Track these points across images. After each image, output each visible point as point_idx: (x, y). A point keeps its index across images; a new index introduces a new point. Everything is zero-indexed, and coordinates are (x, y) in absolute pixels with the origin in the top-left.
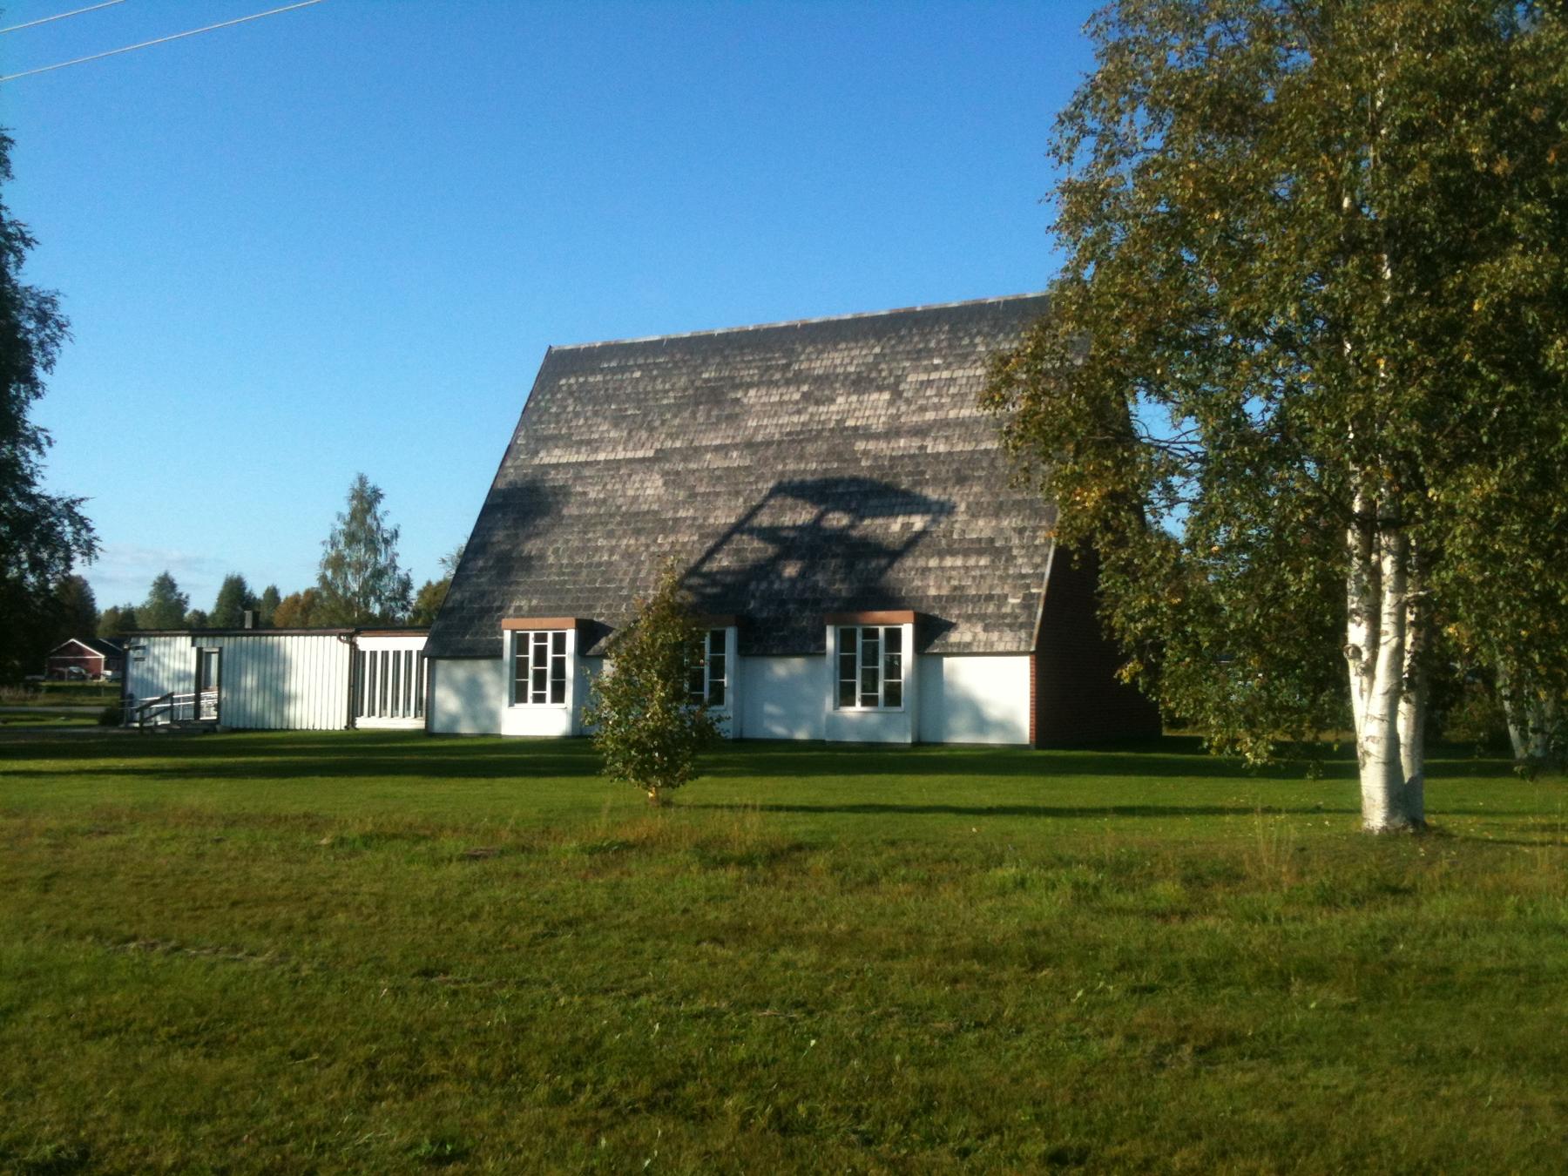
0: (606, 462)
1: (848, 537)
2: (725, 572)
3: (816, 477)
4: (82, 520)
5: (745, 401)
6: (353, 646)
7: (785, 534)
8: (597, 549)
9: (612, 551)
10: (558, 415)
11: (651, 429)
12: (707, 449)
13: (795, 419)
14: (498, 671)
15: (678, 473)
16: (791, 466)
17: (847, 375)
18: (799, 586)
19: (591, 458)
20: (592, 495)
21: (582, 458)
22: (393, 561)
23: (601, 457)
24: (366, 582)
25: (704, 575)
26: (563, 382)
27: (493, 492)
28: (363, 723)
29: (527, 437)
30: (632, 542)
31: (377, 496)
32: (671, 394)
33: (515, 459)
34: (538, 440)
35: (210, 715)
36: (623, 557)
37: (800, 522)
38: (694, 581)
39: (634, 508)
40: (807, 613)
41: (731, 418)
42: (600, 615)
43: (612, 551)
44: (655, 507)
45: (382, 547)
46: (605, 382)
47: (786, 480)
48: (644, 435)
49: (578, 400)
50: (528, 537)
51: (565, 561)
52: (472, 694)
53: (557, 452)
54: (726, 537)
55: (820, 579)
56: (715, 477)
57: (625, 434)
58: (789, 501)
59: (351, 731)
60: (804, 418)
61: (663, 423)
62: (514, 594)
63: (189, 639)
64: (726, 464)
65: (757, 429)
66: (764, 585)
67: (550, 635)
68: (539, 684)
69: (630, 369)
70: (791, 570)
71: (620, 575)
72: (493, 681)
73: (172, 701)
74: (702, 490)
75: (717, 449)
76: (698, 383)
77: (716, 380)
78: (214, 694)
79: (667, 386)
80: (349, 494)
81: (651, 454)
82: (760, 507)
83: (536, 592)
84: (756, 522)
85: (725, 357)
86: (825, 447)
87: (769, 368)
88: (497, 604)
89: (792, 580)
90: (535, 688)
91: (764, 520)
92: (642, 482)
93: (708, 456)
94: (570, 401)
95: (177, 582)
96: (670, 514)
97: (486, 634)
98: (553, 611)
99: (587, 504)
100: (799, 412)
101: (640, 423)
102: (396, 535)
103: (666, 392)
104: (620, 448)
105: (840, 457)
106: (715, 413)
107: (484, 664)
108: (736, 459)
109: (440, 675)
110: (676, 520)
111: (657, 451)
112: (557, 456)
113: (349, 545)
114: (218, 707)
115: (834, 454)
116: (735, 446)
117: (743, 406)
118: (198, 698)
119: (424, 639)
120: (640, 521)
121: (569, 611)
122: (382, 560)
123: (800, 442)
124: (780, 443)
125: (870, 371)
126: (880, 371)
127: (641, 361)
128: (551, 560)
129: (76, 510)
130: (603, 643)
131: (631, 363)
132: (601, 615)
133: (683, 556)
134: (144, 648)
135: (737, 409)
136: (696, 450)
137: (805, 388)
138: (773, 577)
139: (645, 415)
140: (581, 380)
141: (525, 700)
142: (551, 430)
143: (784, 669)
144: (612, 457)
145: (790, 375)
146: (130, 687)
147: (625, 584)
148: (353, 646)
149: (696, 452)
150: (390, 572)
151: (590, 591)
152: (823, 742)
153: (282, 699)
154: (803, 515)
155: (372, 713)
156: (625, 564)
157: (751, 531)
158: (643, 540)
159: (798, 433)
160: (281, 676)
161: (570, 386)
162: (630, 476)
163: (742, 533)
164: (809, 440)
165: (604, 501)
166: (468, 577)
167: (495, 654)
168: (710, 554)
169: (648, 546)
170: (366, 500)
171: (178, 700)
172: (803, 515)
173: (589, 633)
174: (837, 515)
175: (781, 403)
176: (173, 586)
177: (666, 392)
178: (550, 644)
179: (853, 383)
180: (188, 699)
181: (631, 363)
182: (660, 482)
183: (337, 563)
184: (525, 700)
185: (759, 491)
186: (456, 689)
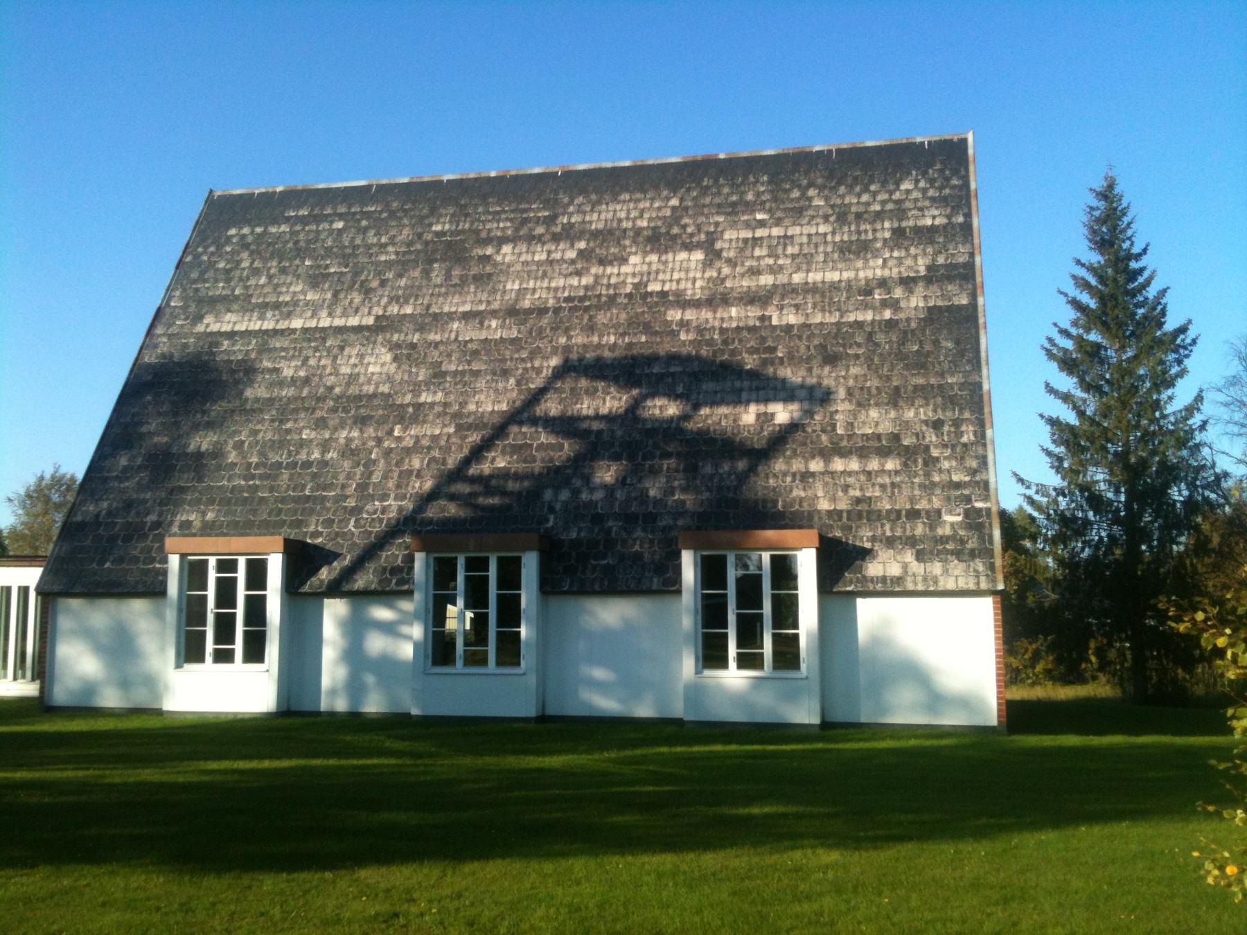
14: (160, 616)
50: (196, 427)
52: (119, 649)
62: (178, 504)
68: (225, 629)
72: (151, 628)
83: (211, 501)
88: (152, 518)
109: (64, 622)
128: (232, 457)
130: (325, 574)
165: (307, 381)
167: (155, 590)
178: (241, 575)
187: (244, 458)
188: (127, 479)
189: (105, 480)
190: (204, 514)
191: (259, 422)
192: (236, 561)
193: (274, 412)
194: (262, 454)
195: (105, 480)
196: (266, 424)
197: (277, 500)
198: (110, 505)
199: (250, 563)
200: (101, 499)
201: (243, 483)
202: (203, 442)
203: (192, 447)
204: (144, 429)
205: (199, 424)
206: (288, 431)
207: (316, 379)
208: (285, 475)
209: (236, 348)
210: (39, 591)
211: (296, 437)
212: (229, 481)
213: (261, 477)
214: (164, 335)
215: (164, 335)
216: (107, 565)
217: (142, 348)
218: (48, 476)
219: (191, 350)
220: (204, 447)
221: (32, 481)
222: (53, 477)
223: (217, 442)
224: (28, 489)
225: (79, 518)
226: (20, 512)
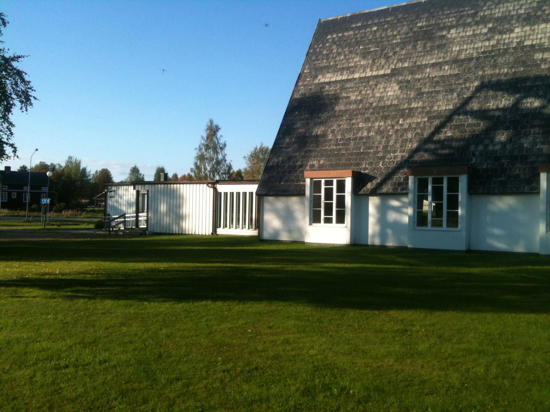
0: (360, 78)
1: (541, 114)
2: (451, 139)
3: (508, 77)
4: (19, 73)
5: (449, 36)
6: (215, 190)
7: (491, 114)
8: (359, 129)
9: (369, 130)
10: (327, 55)
11: (387, 58)
12: (426, 66)
13: (487, 44)
14: (303, 203)
15: (408, 82)
16: (489, 72)
17: (519, 16)
18: (509, 147)
19: (351, 77)
20: (353, 98)
21: (345, 77)
22: (224, 157)
23: (357, 76)
24: (213, 166)
25: (436, 142)
26: (329, 37)
27: (292, 100)
28: (221, 231)
29: (310, 69)
30: (382, 124)
31: (217, 129)
32: (398, 37)
33: (304, 81)
34: (316, 70)
35: (143, 226)
36: (377, 133)
37: (501, 106)
38: (432, 146)
39: (381, 104)
40: (518, 165)
41: (440, 47)
42: (365, 168)
43: (369, 130)
44: (395, 102)
45: (219, 151)
46: (354, 35)
47: (486, 80)
48: (383, 61)
49: (339, 46)
50: (316, 125)
52: (288, 217)
53: (329, 75)
54: (449, 118)
55: (526, 143)
56: (435, 82)
57: (371, 62)
58: (491, 93)
59: (215, 236)
60: (492, 43)
61: (395, 53)
62: (309, 157)
63: (132, 187)
64: (441, 74)
65: (460, 51)
66: (481, 148)
67: (335, 181)
68: (328, 210)
69: (370, 26)
70: (502, 137)
71: (376, 143)
72: (300, 208)
73: (125, 218)
74: (427, 90)
75: (433, 65)
76: (415, 29)
77: (427, 26)
78: (145, 214)
79: (395, 33)
80: (206, 128)
81: (389, 71)
82: (470, 99)
83: (322, 156)
84: (468, 108)
85: (431, 13)
86: (512, 59)
87: (462, 17)
88: (299, 163)
89: (503, 144)
90: (325, 214)
91: (475, 105)
92: (385, 88)
93: (428, 70)
94: (334, 47)
95: (139, 169)
96: (406, 106)
97: (293, 181)
98: (334, 167)
99: (350, 103)
100: (489, 40)
101: (383, 53)
102: (225, 144)
103: (395, 36)
104: (368, 70)
105: (524, 63)
106: (429, 45)
107: (295, 199)
108: (447, 70)
109: (267, 206)
110: (411, 109)
111: (392, 70)
112: (329, 77)
113: (206, 150)
114: (147, 221)
115: (517, 62)
116: (446, 63)
117: (448, 39)
118: (137, 217)
120: (384, 111)
121: (345, 166)
123: (493, 57)
124: (478, 59)
125: (536, 12)
126: (544, 11)
127: (376, 21)
128: (330, 137)
129: (14, 64)
130: (369, 186)
131: (370, 22)
132: (365, 169)
133: (419, 131)
134: (114, 191)
135: (444, 42)
136: (419, 67)
137: (490, 25)
138: (487, 141)
139: (383, 50)
140: (340, 35)
141: (320, 222)
142: (324, 63)
143: (504, 203)
144: (363, 75)
145: (478, 19)
146: (108, 210)
147: (380, 149)
148: (215, 190)
149: (420, 68)
150: (223, 162)
151: (357, 154)
152: (537, 255)
153: (180, 217)
154: (505, 101)
155: (225, 226)
156: (378, 138)
157: (466, 113)
158: (389, 122)
159: (490, 52)
160: (179, 206)
161: (333, 39)
162: (376, 85)
163: (459, 114)
164: (499, 55)
165: (361, 101)
166: (281, 148)
167: (301, 193)
168: (438, 130)
169: (393, 126)
170: (213, 130)
171: (128, 217)
172: (505, 101)
173: (360, 180)
174: (529, 100)
175: (475, 35)
176: (138, 171)
177: (395, 36)
178: (335, 187)
179: (525, 19)
180: (133, 217)
181: (370, 22)
182: (397, 88)
183: (201, 158)
184: (319, 221)
185: (468, 89)
186: (276, 212)
188: (289, 148)
190: (319, 161)
191: (341, 121)
195: (281, 148)
196: (344, 121)
198: (283, 158)
199: (338, 182)
200: (279, 156)
201: (335, 147)
202: (319, 130)
203: (314, 133)
204: (295, 126)
206: (353, 124)
207: (365, 100)
208: (352, 143)
209: (331, 89)
210: (257, 194)
211: (357, 126)
215: (302, 85)
216: (282, 183)
218: (258, 148)
219: (313, 91)
221: (253, 149)
223: (324, 130)
225: (271, 164)
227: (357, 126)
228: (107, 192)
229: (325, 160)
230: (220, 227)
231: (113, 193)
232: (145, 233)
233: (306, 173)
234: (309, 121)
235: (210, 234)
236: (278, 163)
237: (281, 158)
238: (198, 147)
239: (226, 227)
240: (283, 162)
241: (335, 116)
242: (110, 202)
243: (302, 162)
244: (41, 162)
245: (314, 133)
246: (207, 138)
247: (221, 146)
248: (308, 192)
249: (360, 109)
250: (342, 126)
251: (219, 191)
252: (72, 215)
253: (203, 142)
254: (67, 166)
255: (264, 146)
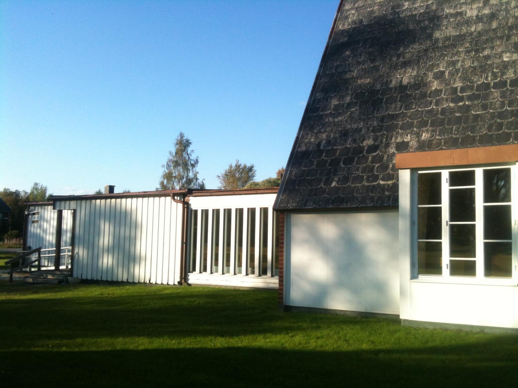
6: (186, 205)
14: (393, 230)
22: (196, 175)
27: (334, 35)
28: (196, 278)
45: (190, 168)
50: (395, 67)
51: (459, 84)
52: (349, 258)
62: (391, 129)
67: (479, 174)
68: (462, 241)
72: (382, 241)
83: (423, 124)
88: (369, 142)
90: (453, 252)
102: (197, 162)
113: (175, 167)
119: (276, 195)
122: (191, 175)
128: (435, 85)
134: (38, 213)
148: (186, 205)
150: (195, 181)
165: (493, 16)
167: (384, 202)
170: (183, 145)
171: (45, 253)
183: (169, 176)
187: (446, 84)
188: (340, 114)
189: (321, 117)
190: (418, 135)
191: (454, 55)
192: (473, 173)
193: (468, 45)
194: (464, 79)
195: (321, 117)
196: (462, 55)
197: (493, 116)
198: (328, 136)
199: (489, 176)
200: (319, 132)
201: (452, 105)
202: (406, 77)
203: (393, 83)
204: (348, 76)
205: (396, 65)
206: (487, 58)
207: (503, 13)
208: (496, 94)
209: (417, 5)
210: (274, 209)
211: (497, 61)
212: (437, 104)
213: (470, 98)
214: (352, 9)
215: (352, 9)
216: (334, 184)
217: (335, 21)
218: (234, 165)
219: (377, 14)
220: (405, 81)
221: (228, 168)
222: (236, 166)
223: (418, 76)
224: (226, 172)
225: (303, 148)
226: (223, 182)
227: (497, 61)
228: (29, 214)
229: (433, 131)
230: (194, 270)
231: (36, 216)
232: (67, 282)
233: (399, 158)
234: (377, 64)
235: (176, 283)
236: (319, 145)
237: (324, 136)
238: (166, 164)
239: (205, 270)
240: (329, 142)
241: (438, 48)
242: (32, 230)
243: (375, 140)
244: (5, 189)
245: (393, 83)
246: (176, 153)
247: (192, 162)
248: (405, 198)
249: (494, 30)
250: (460, 64)
251: (193, 207)
252: (15, 244)
253: (171, 158)
254: (32, 192)
255: (239, 163)
